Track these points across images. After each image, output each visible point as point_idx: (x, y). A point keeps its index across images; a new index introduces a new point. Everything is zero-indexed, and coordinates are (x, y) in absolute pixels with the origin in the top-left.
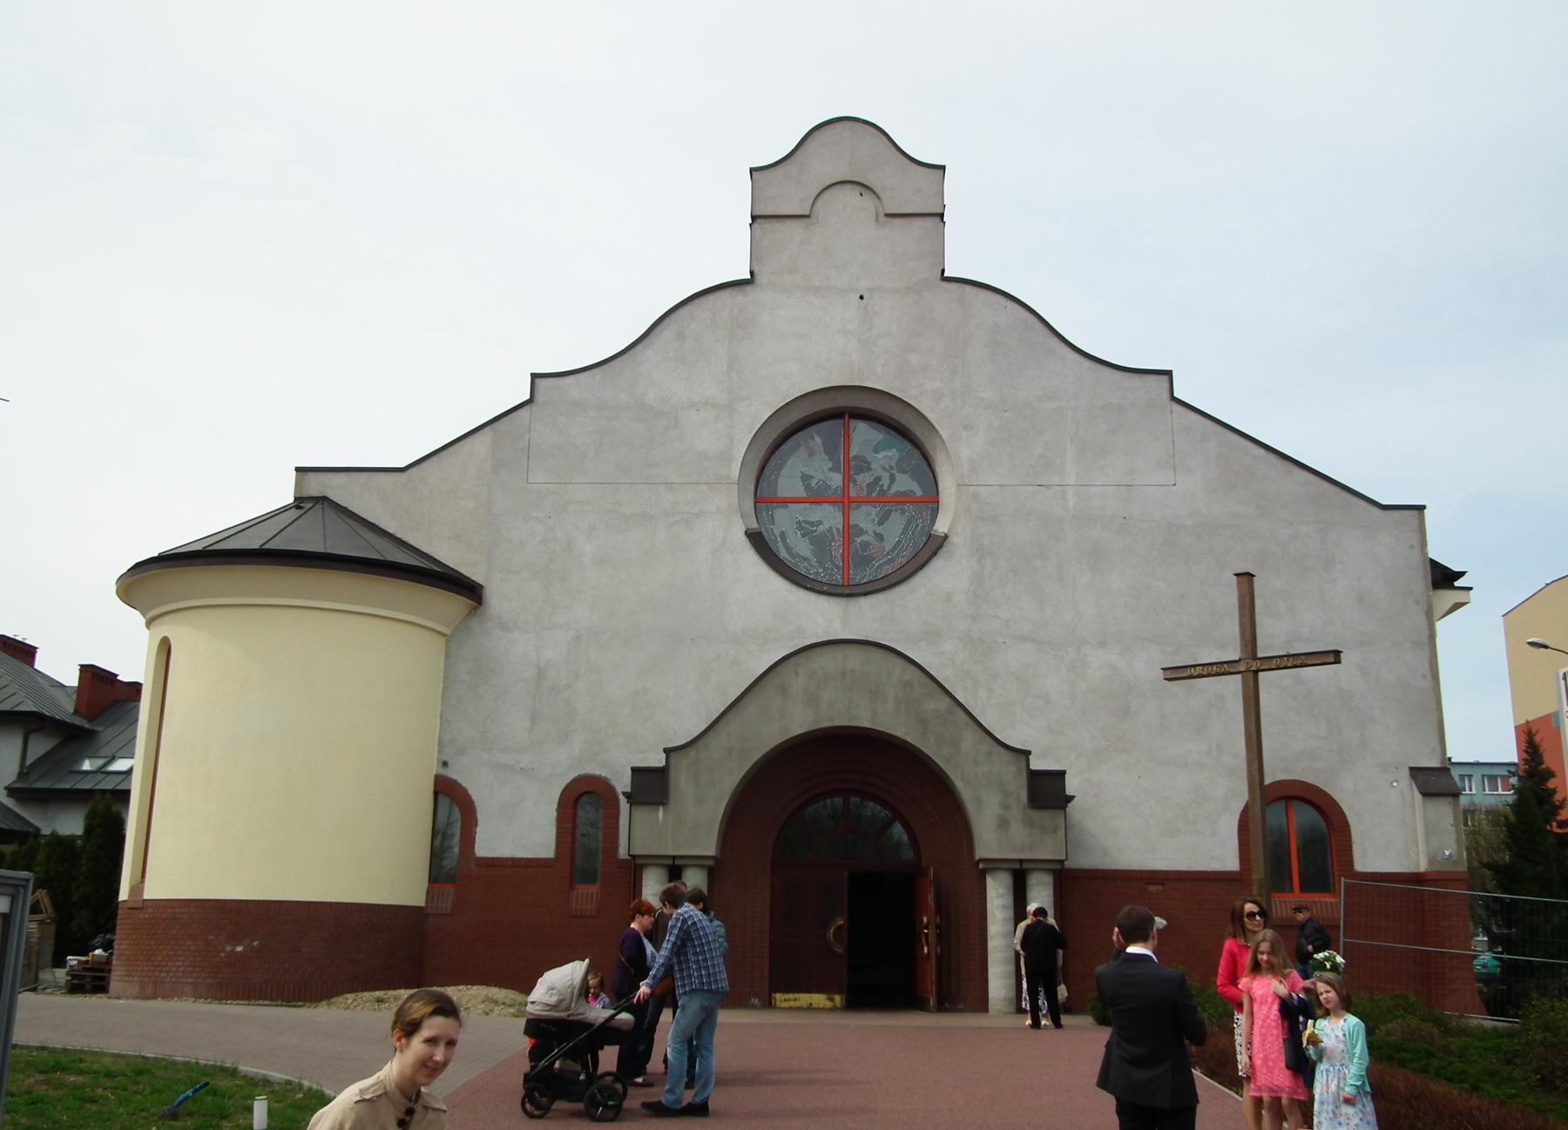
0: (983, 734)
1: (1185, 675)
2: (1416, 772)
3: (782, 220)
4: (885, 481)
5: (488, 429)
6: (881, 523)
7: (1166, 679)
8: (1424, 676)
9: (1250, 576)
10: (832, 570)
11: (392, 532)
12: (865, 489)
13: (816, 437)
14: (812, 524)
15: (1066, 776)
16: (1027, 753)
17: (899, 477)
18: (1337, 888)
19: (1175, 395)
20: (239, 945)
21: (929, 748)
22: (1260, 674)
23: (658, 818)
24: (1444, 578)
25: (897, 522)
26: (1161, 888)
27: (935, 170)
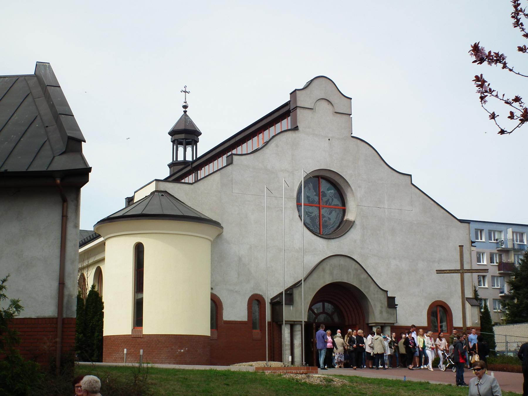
0: (376, 285)
1: (443, 272)
3: (305, 109)
14: (310, 213)
16: (387, 292)
19: (412, 183)
23: (291, 309)
25: (334, 214)
27: (349, 99)
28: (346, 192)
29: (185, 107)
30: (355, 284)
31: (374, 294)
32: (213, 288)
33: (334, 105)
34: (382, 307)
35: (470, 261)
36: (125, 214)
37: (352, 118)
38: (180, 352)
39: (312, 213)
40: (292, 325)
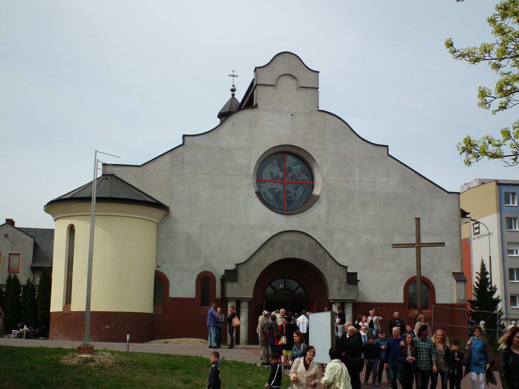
1: (399, 247)
2: (454, 274)
4: (297, 176)
5: (169, 153)
6: (296, 189)
7: (393, 248)
8: (457, 245)
9: (419, 219)
10: (280, 205)
11: (137, 188)
12: (291, 178)
13: (275, 160)
15: (358, 274)
16: (346, 267)
17: (301, 174)
18: (431, 308)
19: (389, 154)
20: (107, 326)
21: (317, 265)
22: (421, 248)
23: (234, 286)
24: (464, 214)
25: (301, 189)
26: (381, 308)
28: (312, 167)
29: (233, 90)
30: (309, 260)
31: (331, 270)
32: (160, 266)
33: (298, 80)
34: (340, 283)
35: (459, 234)
36: (73, 196)
37: (319, 91)
38: (105, 328)
39: (275, 189)
40: (238, 302)
